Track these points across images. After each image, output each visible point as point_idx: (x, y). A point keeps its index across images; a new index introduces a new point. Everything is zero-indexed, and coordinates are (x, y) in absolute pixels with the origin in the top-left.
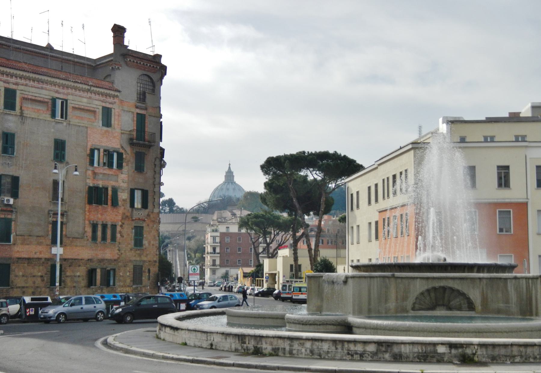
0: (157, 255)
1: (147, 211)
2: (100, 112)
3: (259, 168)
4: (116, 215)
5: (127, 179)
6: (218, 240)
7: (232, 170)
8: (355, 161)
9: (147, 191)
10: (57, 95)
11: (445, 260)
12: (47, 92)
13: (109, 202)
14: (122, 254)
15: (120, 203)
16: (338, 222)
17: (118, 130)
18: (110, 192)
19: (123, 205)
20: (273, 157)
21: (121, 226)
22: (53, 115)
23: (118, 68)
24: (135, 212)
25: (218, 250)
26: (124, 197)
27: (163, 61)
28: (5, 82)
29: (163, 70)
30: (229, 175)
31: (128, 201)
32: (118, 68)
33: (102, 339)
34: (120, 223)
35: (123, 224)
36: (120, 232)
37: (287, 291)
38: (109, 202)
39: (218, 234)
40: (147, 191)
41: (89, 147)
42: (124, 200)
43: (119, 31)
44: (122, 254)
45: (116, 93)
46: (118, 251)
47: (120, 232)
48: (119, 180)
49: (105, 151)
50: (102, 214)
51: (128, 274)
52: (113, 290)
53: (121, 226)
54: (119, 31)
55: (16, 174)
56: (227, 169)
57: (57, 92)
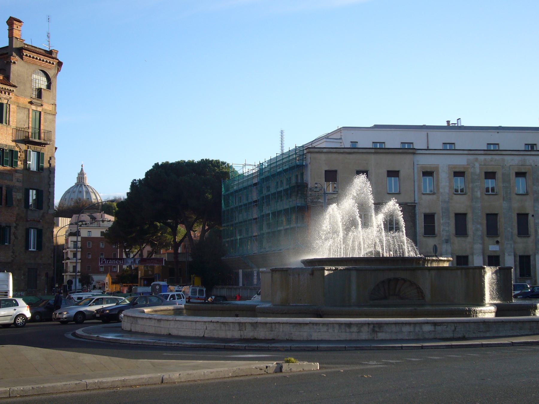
0: (51, 257)
1: (42, 211)
4: (11, 216)
5: (21, 178)
6: (79, 245)
7: (85, 171)
8: (167, 163)
9: (42, 191)
13: (4, 202)
14: (16, 256)
15: (14, 203)
16: (486, 186)
18: (4, 192)
19: (17, 206)
20: (184, 161)
21: (16, 227)
24: (29, 212)
25: (79, 256)
26: (18, 198)
30: (81, 176)
31: (23, 201)
34: (14, 224)
35: (17, 225)
36: (14, 234)
37: (490, 193)
38: (4, 202)
39: (79, 239)
40: (42, 191)
42: (18, 200)
44: (16, 256)
45: (12, 89)
46: (12, 254)
47: (14, 234)
48: (14, 178)
51: (22, 277)
52: (394, 210)
53: (16, 227)
56: (79, 171)
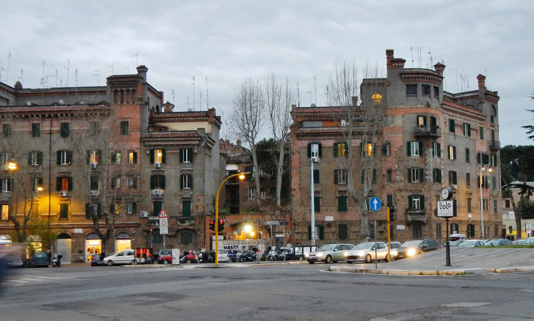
2: (479, 130)
3: (17, 81)
10: (465, 121)
11: (215, 170)
12: (461, 120)
17: (486, 141)
22: (464, 134)
23: (389, 85)
27: (498, 95)
28: (449, 115)
29: (498, 98)
32: (389, 85)
33: (452, 271)
41: (477, 152)
43: (481, 78)
49: (482, 154)
50: (116, 142)
54: (481, 78)
55: (455, 171)
57: (465, 119)
